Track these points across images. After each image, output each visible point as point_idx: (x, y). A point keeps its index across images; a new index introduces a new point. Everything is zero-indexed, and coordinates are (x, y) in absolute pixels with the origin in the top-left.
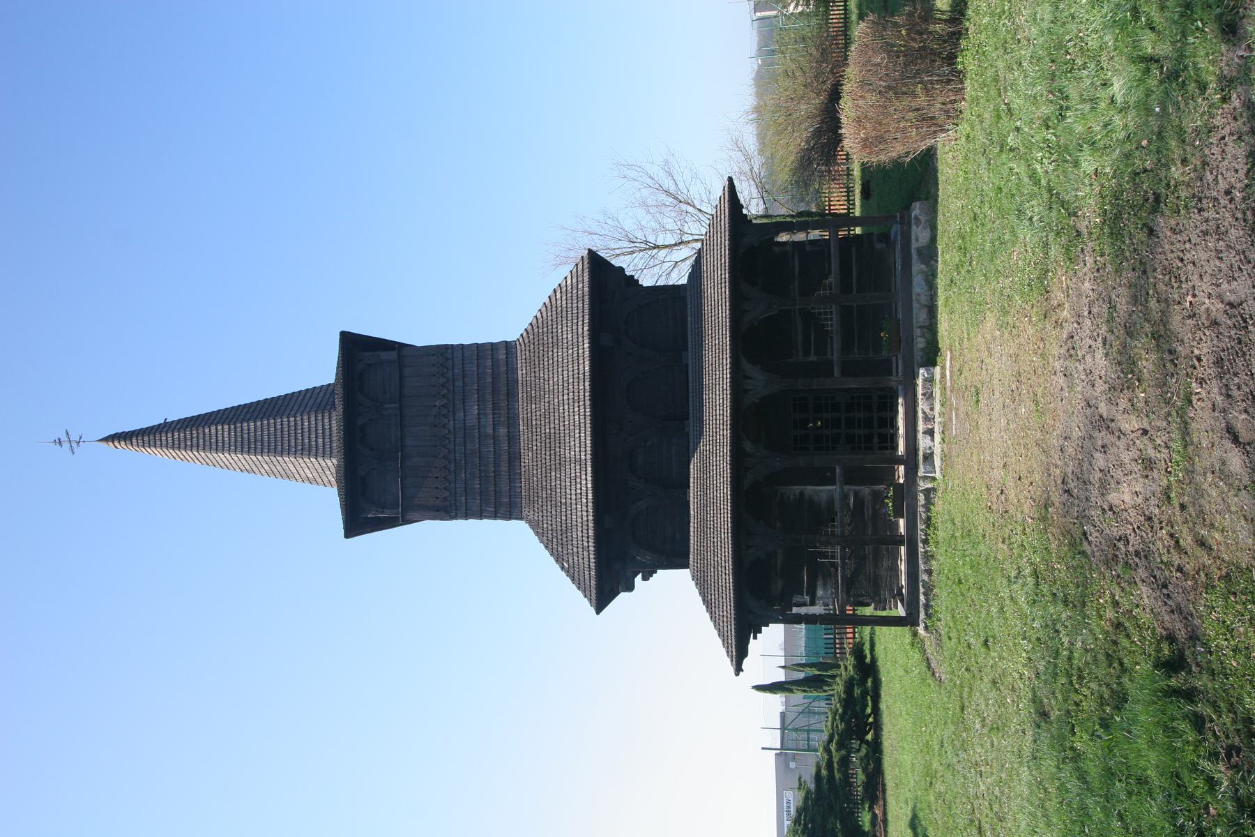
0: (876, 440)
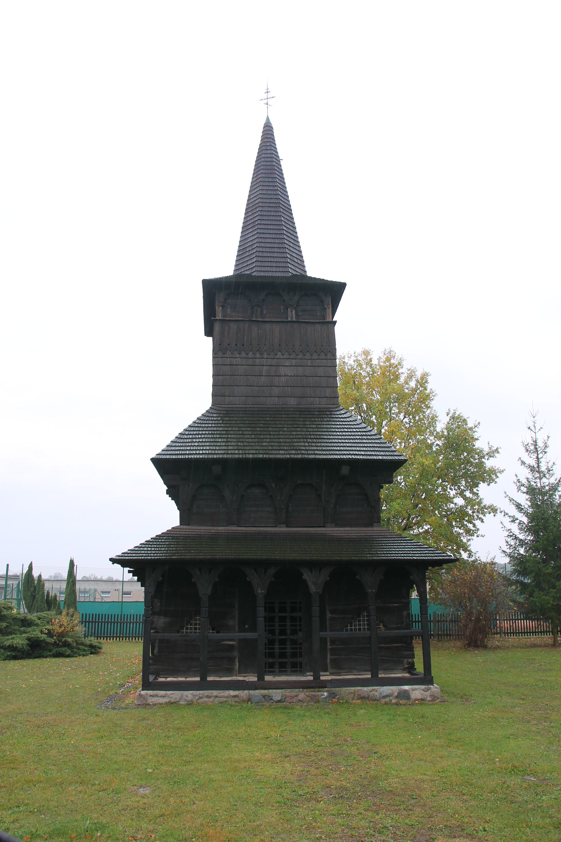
0: (271, 660)
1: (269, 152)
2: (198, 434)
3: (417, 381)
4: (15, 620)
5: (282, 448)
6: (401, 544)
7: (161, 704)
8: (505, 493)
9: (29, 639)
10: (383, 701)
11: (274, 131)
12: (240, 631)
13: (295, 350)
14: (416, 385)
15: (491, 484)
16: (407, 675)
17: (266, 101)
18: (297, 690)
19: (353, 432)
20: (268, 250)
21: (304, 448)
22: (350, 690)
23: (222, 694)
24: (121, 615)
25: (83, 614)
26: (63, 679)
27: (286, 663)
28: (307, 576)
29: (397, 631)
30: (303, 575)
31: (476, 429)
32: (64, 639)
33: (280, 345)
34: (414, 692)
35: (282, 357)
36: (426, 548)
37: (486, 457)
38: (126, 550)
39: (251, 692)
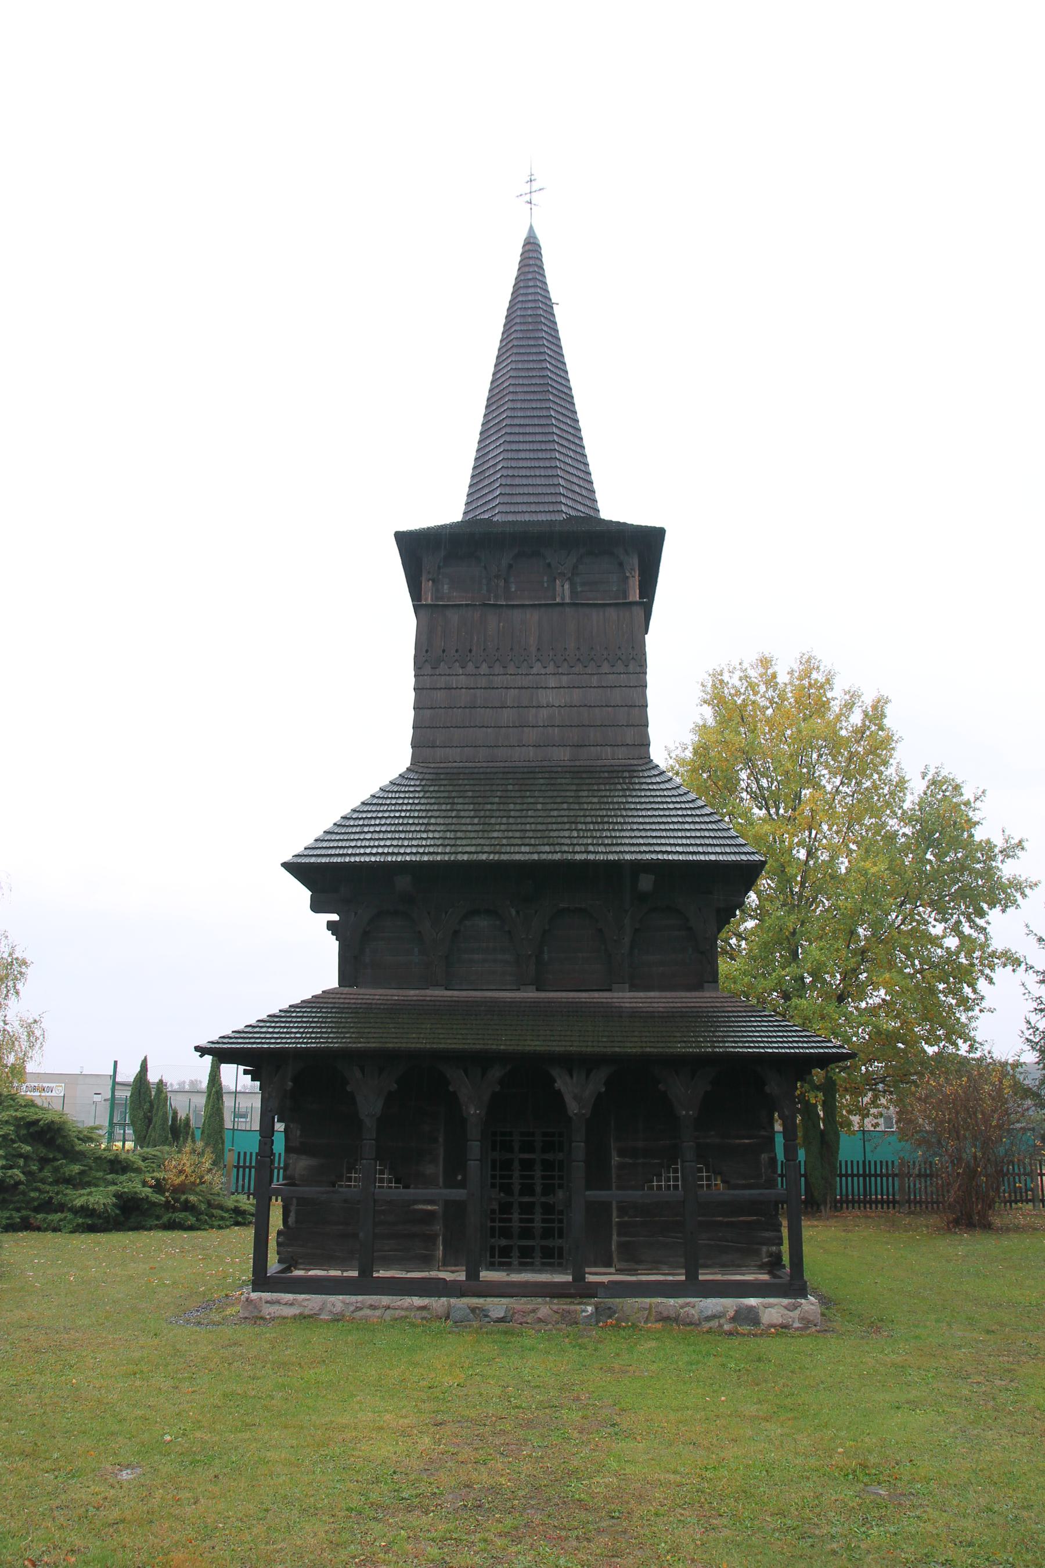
1: (531, 291)
2: (377, 818)
3: (866, 714)
4: (98, 1161)
5: (527, 841)
6: (749, 1024)
7: (285, 1318)
8: (1027, 926)
9: (117, 1195)
10: (706, 1326)
11: (542, 252)
12: (447, 1186)
13: (567, 658)
14: (863, 721)
15: (1008, 910)
16: (765, 1277)
17: (527, 198)
18: (540, 1300)
19: (669, 809)
20: (523, 472)
21: (568, 841)
22: (641, 1303)
23: (399, 1303)
24: (864, 1162)
25: (239, 1153)
26: (151, 1268)
27: (533, 1248)
28: (565, 1084)
29: (747, 1192)
30: (555, 1081)
31: (978, 804)
32: (183, 1197)
33: (538, 649)
34: (767, 1310)
35: (543, 671)
36: (796, 1031)
37: (1000, 857)
38: (228, 1032)
39: (453, 1300)
